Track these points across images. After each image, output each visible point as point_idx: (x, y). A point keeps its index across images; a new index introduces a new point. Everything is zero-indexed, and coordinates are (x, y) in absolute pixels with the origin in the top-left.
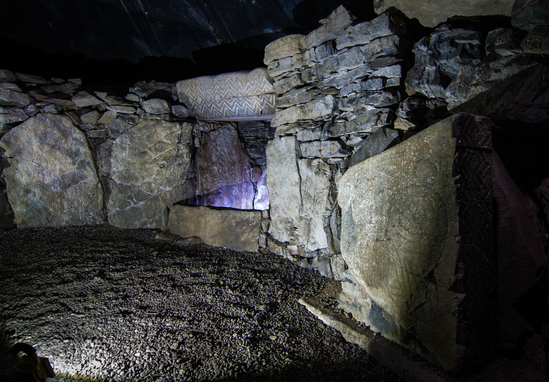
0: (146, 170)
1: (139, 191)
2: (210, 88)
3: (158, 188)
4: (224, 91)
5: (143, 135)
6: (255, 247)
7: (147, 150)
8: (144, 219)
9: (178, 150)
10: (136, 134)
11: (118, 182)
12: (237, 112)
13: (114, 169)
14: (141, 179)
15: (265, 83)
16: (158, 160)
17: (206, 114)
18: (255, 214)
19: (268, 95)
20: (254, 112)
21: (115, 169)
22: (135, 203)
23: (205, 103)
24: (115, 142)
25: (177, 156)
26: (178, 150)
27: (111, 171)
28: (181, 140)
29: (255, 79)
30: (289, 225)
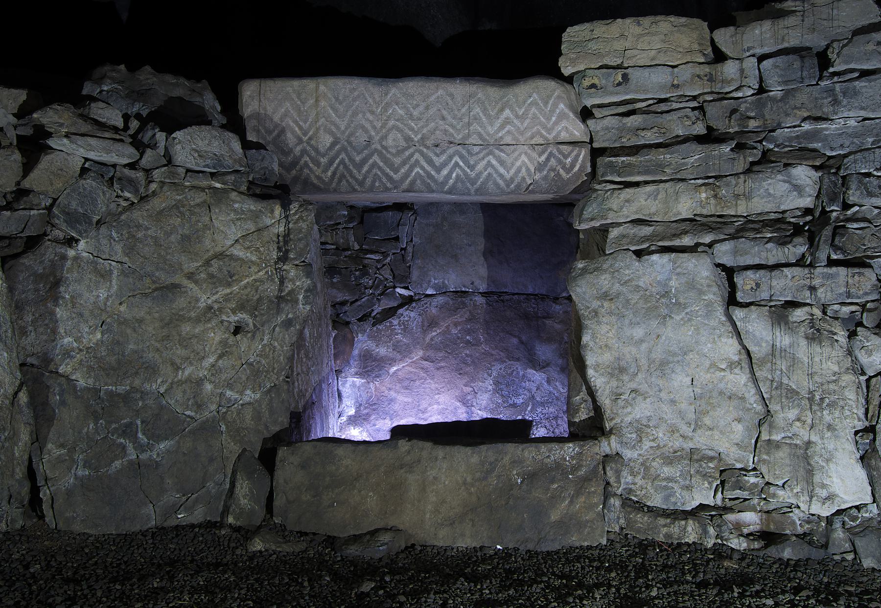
0: (184, 342)
1: (162, 407)
2: (372, 112)
3: (222, 395)
4: (421, 124)
5: (168, 234)
6: (598, 532)
7: (178, 279)
8: (173, 497)
9: (282, 281)
10: (147, 229)
11: (82, 381)
12: (451, 182)
13: (67, 340)
14: (168, 370)
15: (562, 116)
16: (220, 310)
17: (340, 181)
18: (581, 447)
19: (566, 149)
20: (508, 186)
21: (70, 339)
22: (141, 448)
23: (344, 149)
24: (71, 253)
25: (280, 298)
26: (282, 281)
27: (55, 348)
28: (287, 251)
29: (531, 104)
30: (711, 465)
